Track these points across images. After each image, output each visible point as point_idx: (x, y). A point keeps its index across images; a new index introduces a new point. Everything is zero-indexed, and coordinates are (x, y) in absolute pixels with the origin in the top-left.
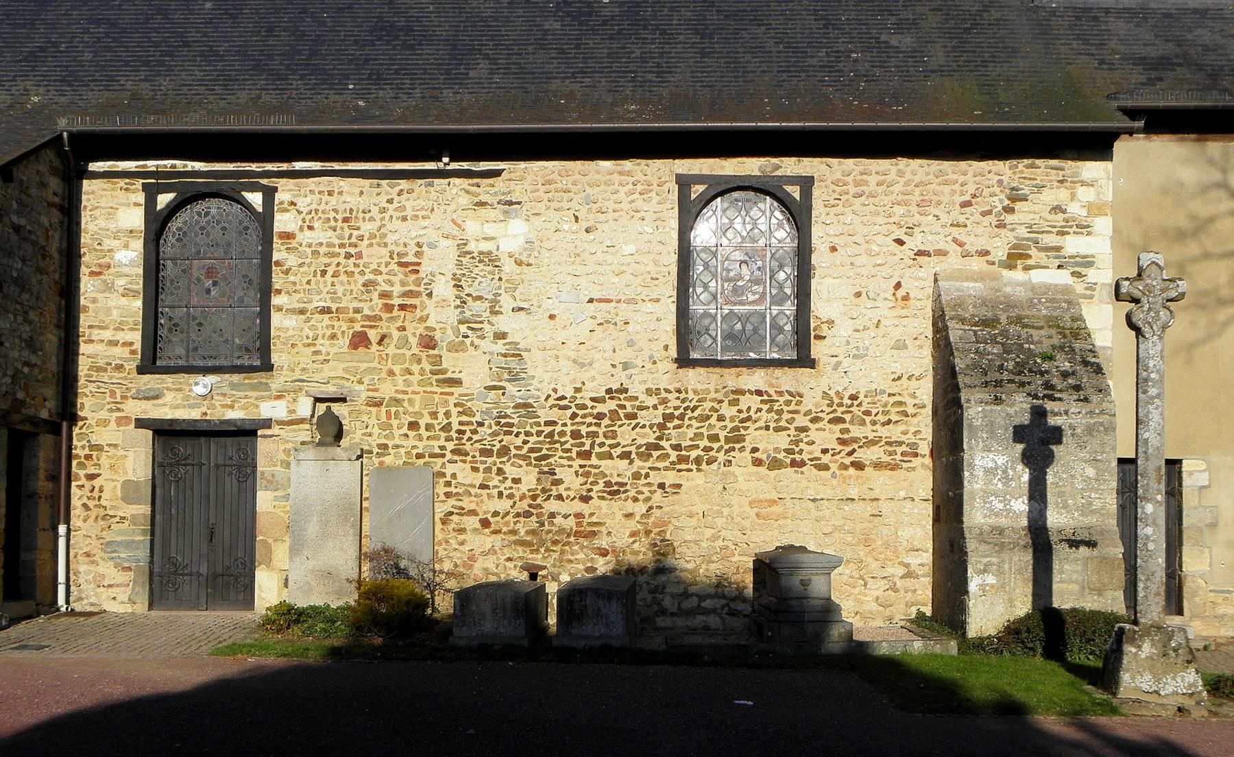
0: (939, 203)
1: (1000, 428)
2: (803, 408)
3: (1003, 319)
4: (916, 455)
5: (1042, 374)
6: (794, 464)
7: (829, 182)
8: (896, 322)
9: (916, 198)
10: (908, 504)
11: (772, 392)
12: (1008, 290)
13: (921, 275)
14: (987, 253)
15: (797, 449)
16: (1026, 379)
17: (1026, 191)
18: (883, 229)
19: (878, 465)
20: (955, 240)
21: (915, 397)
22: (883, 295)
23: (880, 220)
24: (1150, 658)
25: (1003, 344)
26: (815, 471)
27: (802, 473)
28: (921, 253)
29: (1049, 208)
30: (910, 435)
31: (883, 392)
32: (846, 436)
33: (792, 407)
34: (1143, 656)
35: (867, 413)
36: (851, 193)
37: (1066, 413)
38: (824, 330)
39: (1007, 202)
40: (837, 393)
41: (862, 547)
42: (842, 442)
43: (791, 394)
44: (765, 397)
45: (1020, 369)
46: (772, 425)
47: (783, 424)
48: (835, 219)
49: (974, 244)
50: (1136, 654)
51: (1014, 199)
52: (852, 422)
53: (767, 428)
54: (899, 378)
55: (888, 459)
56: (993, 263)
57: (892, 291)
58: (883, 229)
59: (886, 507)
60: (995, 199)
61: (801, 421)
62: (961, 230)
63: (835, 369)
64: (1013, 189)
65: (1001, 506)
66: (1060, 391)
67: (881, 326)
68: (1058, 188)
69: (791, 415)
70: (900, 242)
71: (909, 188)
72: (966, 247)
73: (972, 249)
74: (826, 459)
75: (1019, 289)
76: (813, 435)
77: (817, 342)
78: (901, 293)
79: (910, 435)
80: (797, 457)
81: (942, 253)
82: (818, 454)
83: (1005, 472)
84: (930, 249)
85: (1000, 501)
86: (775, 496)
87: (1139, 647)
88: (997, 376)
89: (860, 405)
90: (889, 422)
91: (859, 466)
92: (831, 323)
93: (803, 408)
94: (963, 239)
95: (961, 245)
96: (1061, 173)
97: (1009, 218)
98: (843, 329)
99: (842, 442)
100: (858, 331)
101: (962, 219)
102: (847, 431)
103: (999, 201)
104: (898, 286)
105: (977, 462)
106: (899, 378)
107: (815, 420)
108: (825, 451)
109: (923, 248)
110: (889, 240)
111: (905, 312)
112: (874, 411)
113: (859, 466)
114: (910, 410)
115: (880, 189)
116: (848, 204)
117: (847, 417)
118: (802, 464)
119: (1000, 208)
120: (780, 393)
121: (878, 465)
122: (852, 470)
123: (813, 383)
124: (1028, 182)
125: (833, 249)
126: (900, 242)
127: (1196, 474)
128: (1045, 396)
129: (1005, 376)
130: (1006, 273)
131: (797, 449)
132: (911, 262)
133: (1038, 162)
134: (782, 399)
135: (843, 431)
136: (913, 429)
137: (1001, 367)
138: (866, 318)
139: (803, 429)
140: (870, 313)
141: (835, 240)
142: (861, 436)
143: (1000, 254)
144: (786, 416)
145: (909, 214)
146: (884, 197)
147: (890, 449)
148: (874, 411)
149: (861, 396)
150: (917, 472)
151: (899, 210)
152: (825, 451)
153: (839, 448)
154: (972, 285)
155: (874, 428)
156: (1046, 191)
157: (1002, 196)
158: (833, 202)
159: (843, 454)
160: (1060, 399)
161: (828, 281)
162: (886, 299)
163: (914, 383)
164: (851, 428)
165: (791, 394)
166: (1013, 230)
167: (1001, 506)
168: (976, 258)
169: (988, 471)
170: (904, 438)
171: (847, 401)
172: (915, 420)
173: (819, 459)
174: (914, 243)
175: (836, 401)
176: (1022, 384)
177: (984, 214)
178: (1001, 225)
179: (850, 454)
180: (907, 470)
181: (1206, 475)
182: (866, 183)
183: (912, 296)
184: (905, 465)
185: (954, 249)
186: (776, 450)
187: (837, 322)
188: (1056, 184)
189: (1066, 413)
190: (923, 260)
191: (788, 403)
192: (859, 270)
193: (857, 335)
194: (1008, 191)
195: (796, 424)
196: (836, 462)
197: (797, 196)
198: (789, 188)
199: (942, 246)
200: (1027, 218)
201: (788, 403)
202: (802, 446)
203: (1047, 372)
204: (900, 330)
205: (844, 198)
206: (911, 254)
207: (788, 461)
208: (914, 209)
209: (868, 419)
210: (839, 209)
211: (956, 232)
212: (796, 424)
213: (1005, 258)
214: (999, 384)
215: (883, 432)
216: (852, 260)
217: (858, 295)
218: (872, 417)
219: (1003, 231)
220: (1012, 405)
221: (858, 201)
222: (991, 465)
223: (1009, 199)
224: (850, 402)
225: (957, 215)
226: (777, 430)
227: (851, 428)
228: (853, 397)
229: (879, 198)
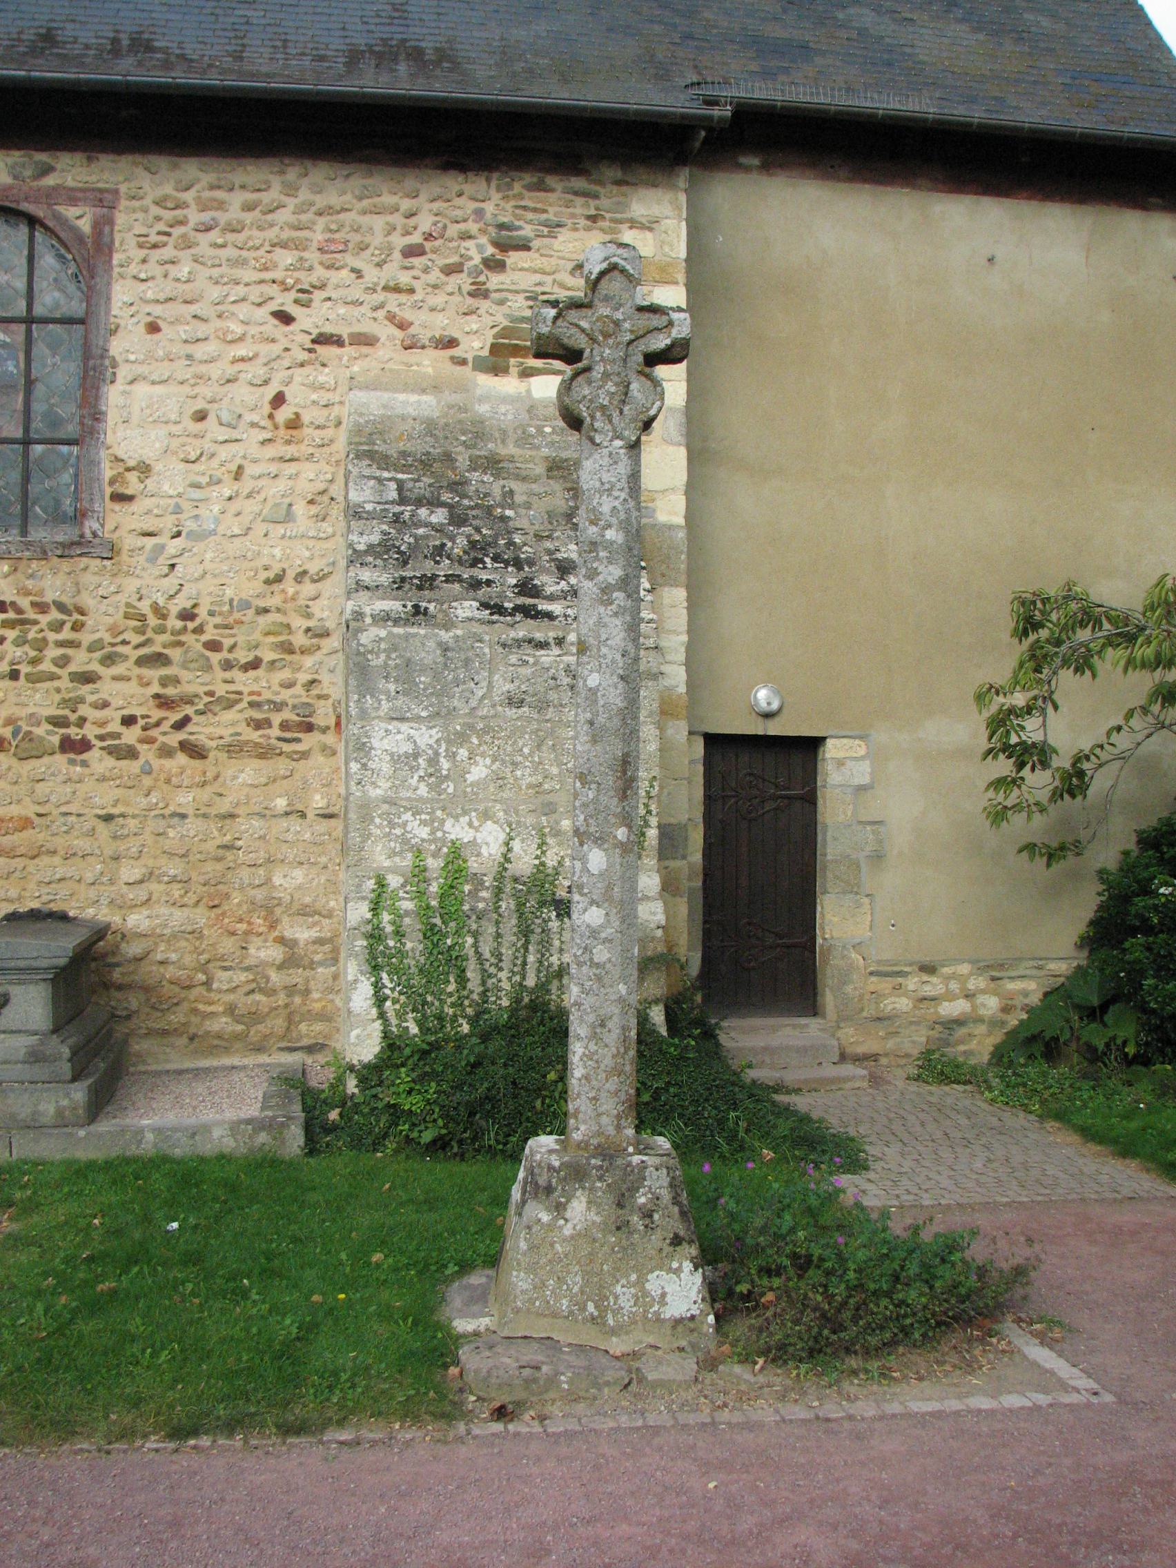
0: (363, 247)
1: (423, 671)
2: (86, 638)
3: (462, 461)
4: (309, 728)
5: (518, 564)
6: (68, 745)
7: (148, 201)
8: (273, 468)
9: (318, 236)
10: (295, 824)
11: (24, 603)
12: (483, 409)
13: (321, 379)
14: (452, 343)
15: (73, 717)
16: (484, 576)
17: (527, 231)
18: (255, 293)
19: (235, 749)
20: (391, 317)
21: (309, 616)
22: (249, 417)
23: (248, 275)
24: (585, 1235)
25: (450, 507)
26: (110, 762)
27: (85, 764)
28: (323, 339)
29: (570, 265)
30: (298, 690)
31: (245, 605)
32: (170, 691)
33: (66, 634)
34: (568, 1231)
35: (214, 646)
36: (191, 224)
37: (560, 642)
38: (133, 484)
39: (490, 250)
40: (156, 608)
41: (201, 909)
42: (164, 702)
43: (61, 607)
44: (11, 615)
45: (476, 553)
46: (24, 669)
47: (46, 666)
48: (158, 271)
49: (430, 324)
50: (551, 1227)
51: (504, 246)
52: (184, 666)
53: (14, 675)
54: (279, 579)
55: (255, 736)
56: (463, 362)
57: (267, 409)
58: (255, 293)
59: (249, 827)
60: (470, 244)
61: (81, 660)
62: (403, 298)
63: (153, 560)
64: (502, 227)
65: (424, 833)
66: (551, 598)
67: (245, 476)
68: (588, 229)
69: (61, 651)
70: (285, 318)
71: (304, 217)
72: (412, 330)
73: (425, 336)
74: (131, 736)
75: (503, 409)
76: (106, 689)
77: (117, 507)
78: (284, 414)
79: (298, 690)
80: (74, 732)
81: (365, 340)
82: (115, 726)
83: (433, 761)
84: (344, 331)
85: (423, 823)
86: (30, 810)
87: (560, 1208)
88: (428, 567)
89: (199, 630)
90: (255, 664)
91: (194, 751)
92: (144, 469)
93: (86, 638)
94: (408, 315)
95: (402, 326)
96: (592, 203)
97: (495, 280)
98: (170, 480)
99: (164, 702)
100: (197, 486)
101: (404, 279)
102: (176, 681)
103: (477, 250)
104: (279, 400)
105: (375, 743)
106: (279, 579)
107: (109, 660)
108: (129, 721)
109: (328, 329)
110: (263, 313)
111: (290, 451)
112: (227, 643)
113: (194, 751)
114: (299, 640)
115: (248, 217)
116: (186, 244)
117: (175, 654)
118: (83, 746)
119: (477, 260)
120: (42, 608)
121: (235, 749)
122: (182, 758)
123: (107, 587)
124: (530, 216)
125: (153, 328)
126: (285, 318)
127: (849, 764)
128: (518, 609)
129: (445, 568)
130: (486, 382)
131: (73, 717)
132: (305, 356)
133: (551, 180)
134: (44, 619)
135: (164, 682)
136: (303, 677)
137: (440, 550)
138: (215, 463)
139: (88, 678)
140: (224, 453)
141: (158, 310)
142: (201, 690)
143: (476, 345)
144: (53, 652)
145: (301, 265)
146: (256, 233)
147: (258, 715)
148: (227, 643)
149: (202, 612)
150: (310, 762)
151: (286, 258)
152: (129, 721)
153: (157, 714)
154: (414, 398)
155: (228, 675)
156: (564, 235)
157: (483, 240)
158: (154, 238)
159: (166, 726)
160: (550, 616)
161: (142, 389)
162: (253, 425)
163: (308, 589)
164: (185, 675)
165: (61, 607)
166: (501, 302)
167: (424, 833)
168: (431, 353)
169: (395, 759)
170: (286, 695)
171: (174, 623)
172: (308, 661)
173: (117, 736)
174: (309, 321)
175: (153, 621)
176: (476, 584)
177: (450, 270)
178: (480, 292)
179: (180, 725)
180: (289, 756)
181: (866, 766)
182: (221, 205)
183: (306, 419)
184: (287, 748)
185: (385, 331)
186: (34, 719)
187: (158, 467)
188: (583, 222)
189: (560, 642)
190: (323, 351)
191: (57, 627)
192: (203, 369)
193: (197, 494)
194: (493, 231)
195: (72, 668)
196: (151, 741)
197: (85, 225)
198: (70, 212)
199: (366, 327)
200: (527, 281)
201: (57, 627)
202: (84, 710)
203: (531, 563)
204: (282, 485)
205: (177, 231)
206: (306, 341)
207: (56, 740)
208: (312, 256)
209: (215, 658)
210: (167, 252)
211: (393, 302)
212: (72, 668)
213: (486, 353)
214: (427, 582)
215: (245, 682)
216: (189, 349)
217: (201, 416)
218: (225, 654)
219: (485, 305)
220: (448, 625)
221: (204, 239)
222: (407, 748)
223: (496, 244)
224: (179, 624)
225: (394, 272)
226: (33, 679)
227: (185, 675)
228: (187, 615)
229: (246, 233)
